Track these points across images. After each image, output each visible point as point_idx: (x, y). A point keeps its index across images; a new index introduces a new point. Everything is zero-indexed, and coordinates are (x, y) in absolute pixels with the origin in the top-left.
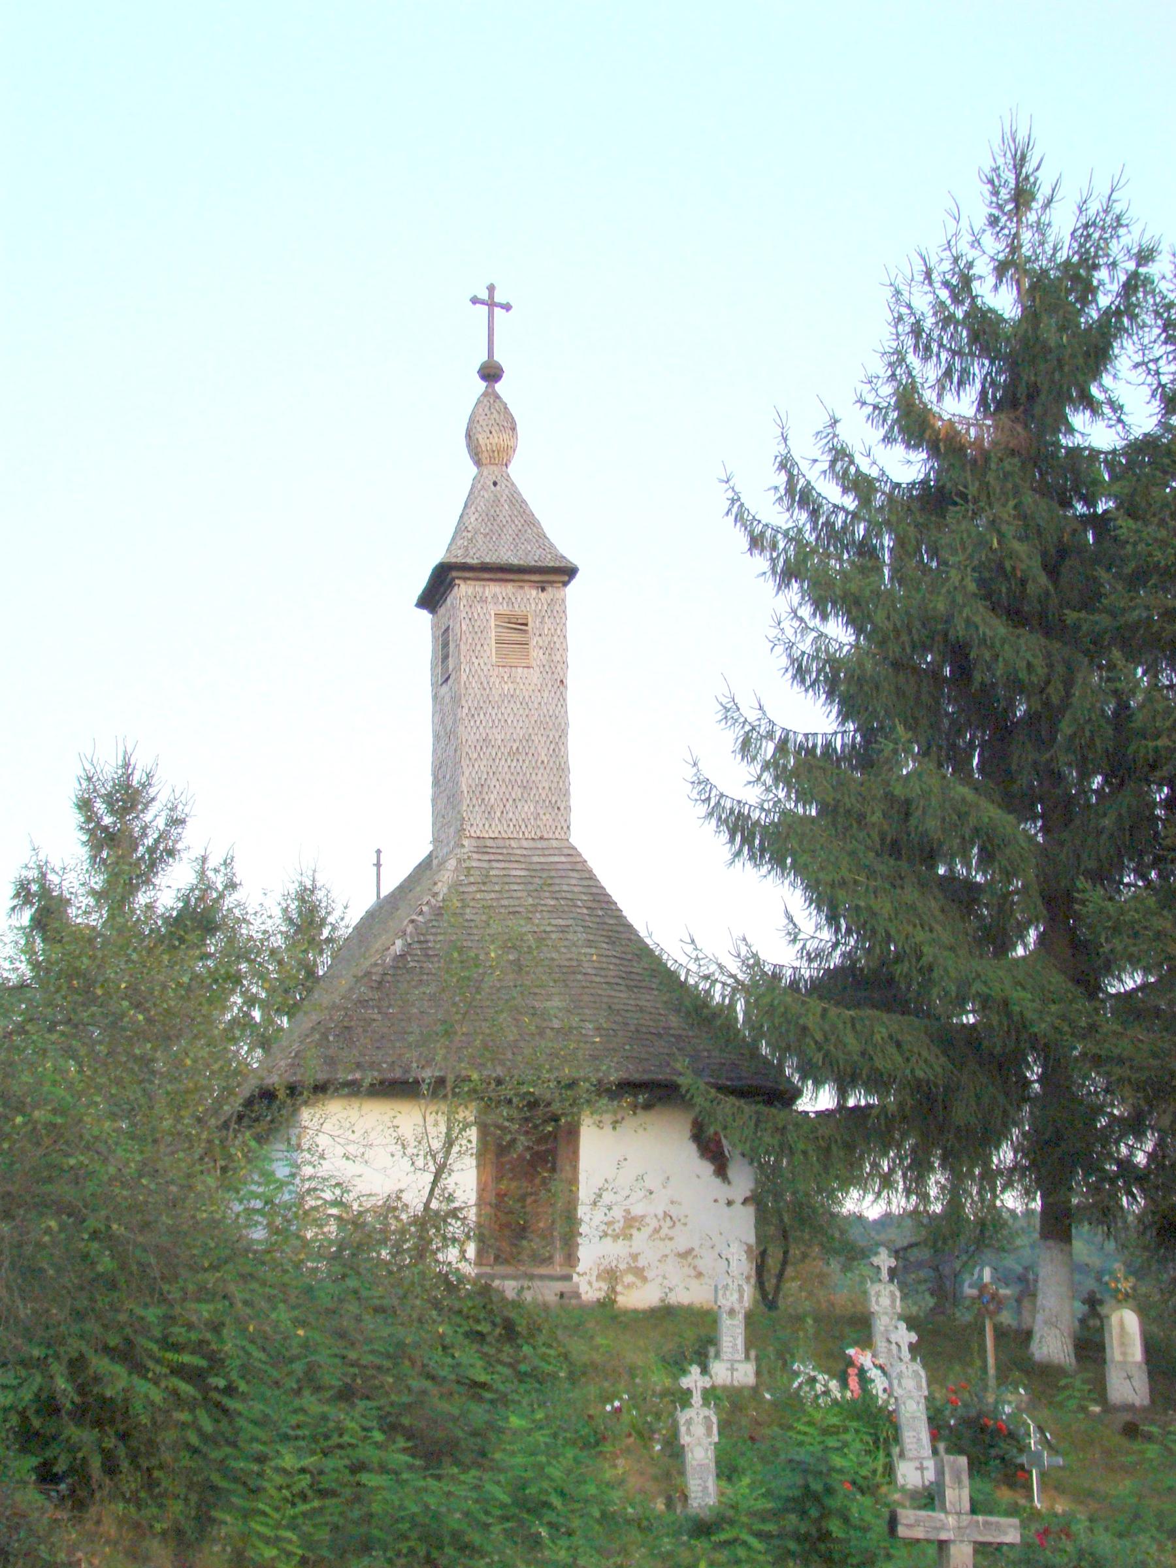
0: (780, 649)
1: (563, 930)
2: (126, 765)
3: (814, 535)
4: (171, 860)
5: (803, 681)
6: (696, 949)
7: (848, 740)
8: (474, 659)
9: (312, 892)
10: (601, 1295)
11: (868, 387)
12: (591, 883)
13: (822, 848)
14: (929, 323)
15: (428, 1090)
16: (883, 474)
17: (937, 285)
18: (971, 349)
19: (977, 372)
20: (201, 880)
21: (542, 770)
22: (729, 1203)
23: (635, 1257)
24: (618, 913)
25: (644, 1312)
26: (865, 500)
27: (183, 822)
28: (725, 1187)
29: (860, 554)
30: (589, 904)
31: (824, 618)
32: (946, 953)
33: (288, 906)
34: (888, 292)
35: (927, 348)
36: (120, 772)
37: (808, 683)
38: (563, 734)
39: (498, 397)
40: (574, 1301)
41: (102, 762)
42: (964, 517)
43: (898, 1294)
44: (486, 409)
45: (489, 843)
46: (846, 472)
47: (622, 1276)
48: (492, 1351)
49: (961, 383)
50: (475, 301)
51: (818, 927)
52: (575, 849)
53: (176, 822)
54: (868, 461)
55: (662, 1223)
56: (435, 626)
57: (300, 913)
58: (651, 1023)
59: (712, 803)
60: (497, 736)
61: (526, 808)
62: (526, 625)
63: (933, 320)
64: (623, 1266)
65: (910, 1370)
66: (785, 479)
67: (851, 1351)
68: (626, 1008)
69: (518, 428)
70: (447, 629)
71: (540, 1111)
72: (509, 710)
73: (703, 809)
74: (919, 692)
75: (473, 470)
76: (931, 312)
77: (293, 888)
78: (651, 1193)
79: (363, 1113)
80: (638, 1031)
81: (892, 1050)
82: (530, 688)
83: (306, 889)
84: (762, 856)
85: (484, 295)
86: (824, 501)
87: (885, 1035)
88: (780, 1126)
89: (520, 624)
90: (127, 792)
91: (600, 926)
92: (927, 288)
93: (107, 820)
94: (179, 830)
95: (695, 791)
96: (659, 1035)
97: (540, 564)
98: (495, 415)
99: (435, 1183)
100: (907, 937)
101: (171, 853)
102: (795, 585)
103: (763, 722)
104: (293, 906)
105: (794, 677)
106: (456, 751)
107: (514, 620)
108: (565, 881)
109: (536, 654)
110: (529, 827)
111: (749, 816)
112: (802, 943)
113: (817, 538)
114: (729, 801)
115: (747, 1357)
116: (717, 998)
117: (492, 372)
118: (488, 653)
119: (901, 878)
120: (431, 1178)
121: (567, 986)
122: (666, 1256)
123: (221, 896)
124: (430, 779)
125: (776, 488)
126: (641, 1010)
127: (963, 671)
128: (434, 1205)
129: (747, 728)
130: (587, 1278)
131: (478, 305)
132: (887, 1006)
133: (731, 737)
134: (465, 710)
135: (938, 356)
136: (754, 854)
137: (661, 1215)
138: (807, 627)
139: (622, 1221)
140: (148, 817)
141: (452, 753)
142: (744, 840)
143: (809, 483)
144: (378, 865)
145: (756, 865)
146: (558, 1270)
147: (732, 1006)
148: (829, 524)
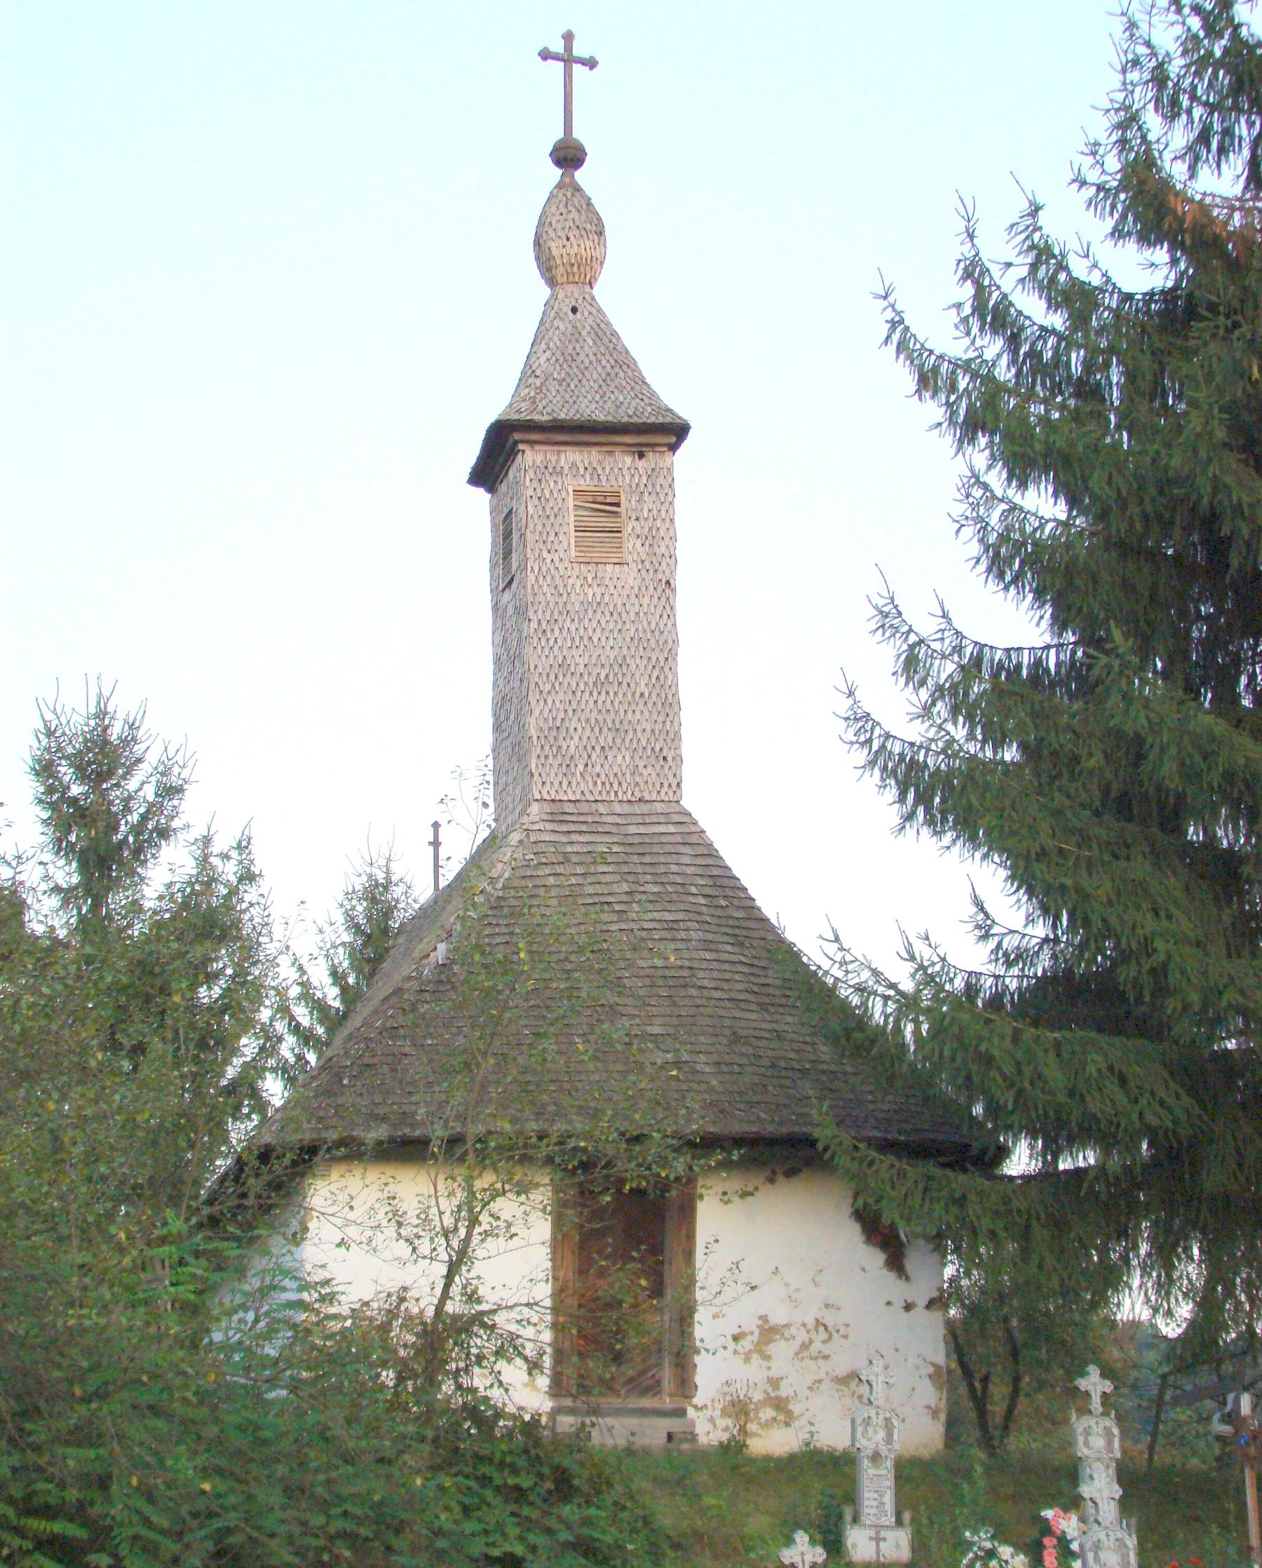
0: (968, 532)
1: (671, 926)
2: (101, 714)
3: (1013, 371)
4: (163, 842)
5: (1001, 576)
6: (841, 949)
7: (1065, 656)
8: (545, 554)
9: (386, 888)
10: (724, 1437)
11: (1091, 160)
12: (710, 862)
13: (1013, 807)
14: (1175, 67)
15: (440, 1147)
16: (1108, 280)
17: (1186, 11)
18: (1235, 102)
19: (1245, 133)
20: (204, 868)
21: (641, 706)
22: (908, 1307)
23: (775, 1383)
24: (749, 903)
25: (778, 1460)
26: (1079, 320)
27: (179, 790)
28: (901, 1283)
29: (1078, 394)
30: (708, 891)
31: (1023, 485)
32: (1187, 949)
33: (353, 908)
34: (1118, 25)
35: (1175, 102)
36: (92, 723)
37: (1008, 578)
38: (671, 655)
39: (577, 189)
40: (685, 1446)
41: (68, 711)
42: (1214, 336)
43: (1116, 1431)
44: (562, 206)
45: (569, 808)
46: (1053, 280)
47: (756, 1410)
48: (535, 1514)
49: (1222, 150)
50: (546, 55)
51: (1030, 920)
52: (688, 814)
53: (170, 791)
54: (1087, 263)
55: (813, 1335)
56: (494, 510)
57: (369, 918)
58: (793, 1055)
59: (875, 747)
60: (578, 659)
61: (620, 758)
62: (618, 505)
63: (1182, 62)
64: (757, 1396)
65: (1112, 1538)
66: (973, 292)
67: (1048, 1513)
68: (757, 1034)
69: (607, 232)
70: (510, 512)
71: (598, 1173)
72: (594, 623)
73: (861, 756)
74: (1154, 586)
75: (546, 292)
76: (1179, 52)
77: (360, 883)
78: (753, 1288)
79: (367, 1181)
80: (773, 1066)
81: (1112, 1086)
82: (625, 593)
83: (377, 885)
84: (944, 820)
85: (558, 47)
86: (1027, 323)
87: (1103, 1066)
88: (957, 1195)
89: (607, 504)
90: (102, 749)
91: (724, 921)
92: (1173, 17)
93: (76, 790)
94: (176, 802)
95: (851, 731)
96: (804, 1072)
97: (635, 420)
98: (574, 214)
99: (449, 1279)
100: (1134, 928)
101: (164, 833)
102: (983, 440)
103: (947, 634)
104: (360, 909)
105: (989, 570)
106: (521, 680)
107: (600, 499)
108: (674, 858)
109: (632, 547)
110: (624, 785)
111: (926, 765)
112: (996, 939)
113: (1018, 374)
114: (898, 743)
115: (899, 1522)
116: (878, 1018)
117: (570, 154)
118: (565, 544)
119: (1128, 846)
120: (443, 1270)
121: (675, 1004)
122: (820, 1381)
123: (234, 891)
124: (490, 721)
125: (959, 306)
126: (779, 1036)
127: (1218, 548)
128: (450, 1307)
129: (913, 638)
130: (708, 1413)
131: (549, 61)
132: (1114, 1027)
133: (889, 654)
134: (534, 625)
135: (1189, 112)
136: (933, 816)
137: (811, 1323)
138: (994, 497)
139: (757, 1332)
140: (132, 785)
141: (517, 685)
142: (919, 799)
143: (1005, 296)
144: (436, 844)
145: (935, 833)
146: (668, 1402)
147: (898, 1030)
148: (1034, 354)
